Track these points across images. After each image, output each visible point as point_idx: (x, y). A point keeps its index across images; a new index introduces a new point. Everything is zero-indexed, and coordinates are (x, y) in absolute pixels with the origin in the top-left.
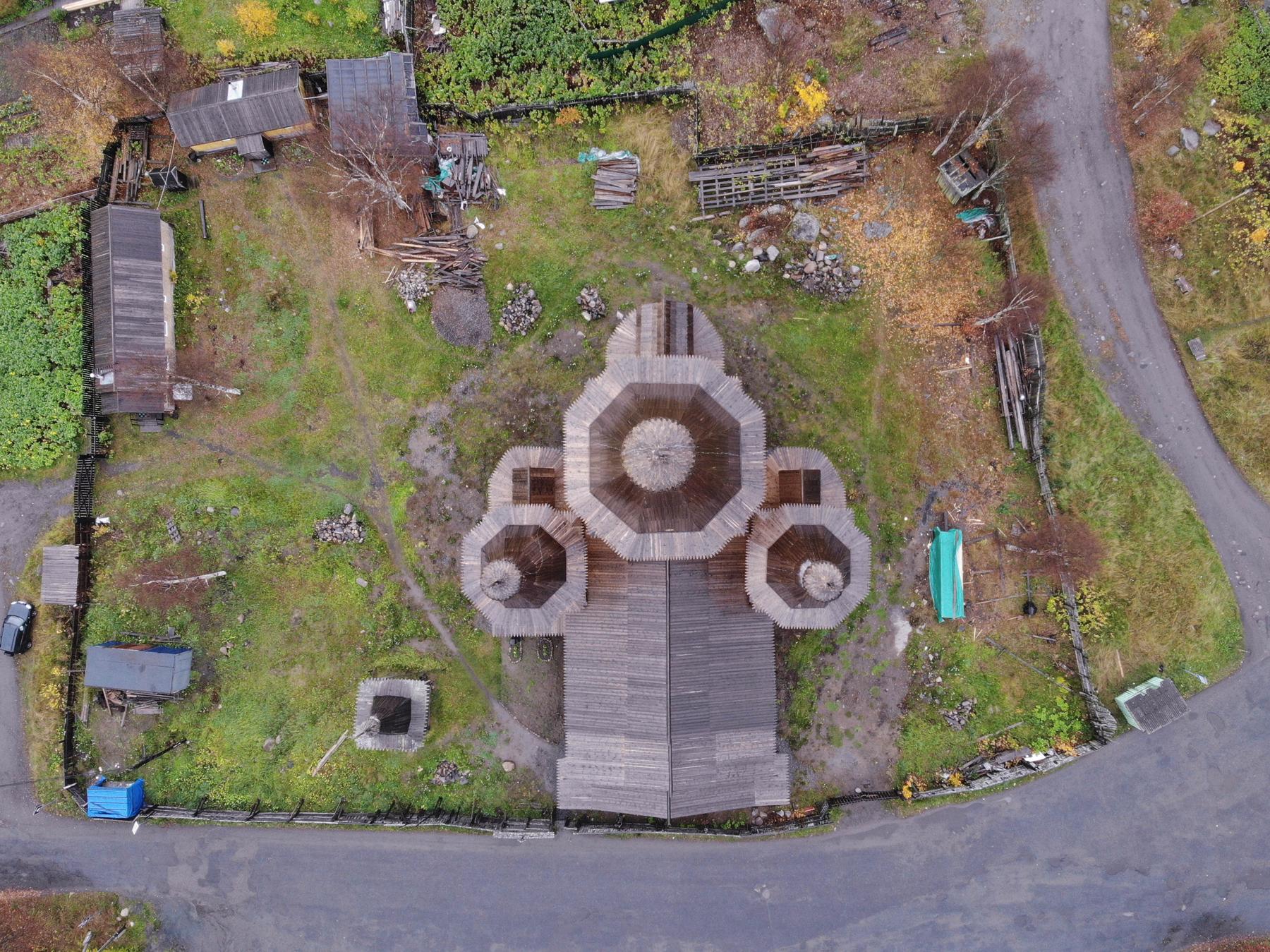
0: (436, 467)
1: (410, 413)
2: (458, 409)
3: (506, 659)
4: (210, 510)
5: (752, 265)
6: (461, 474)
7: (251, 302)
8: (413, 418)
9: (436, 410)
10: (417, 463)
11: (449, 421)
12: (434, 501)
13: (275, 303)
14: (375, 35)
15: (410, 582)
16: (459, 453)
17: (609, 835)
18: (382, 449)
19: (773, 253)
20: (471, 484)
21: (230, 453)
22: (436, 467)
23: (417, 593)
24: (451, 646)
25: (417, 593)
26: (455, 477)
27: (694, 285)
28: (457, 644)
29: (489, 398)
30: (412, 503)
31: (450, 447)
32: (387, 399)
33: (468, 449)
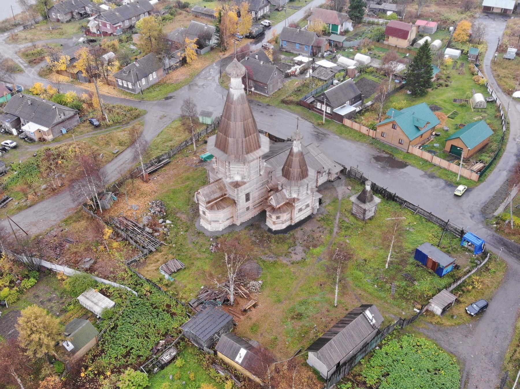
0: (299, 249)
1: (292, 266)
2: (277, 256)
3: (327, 204)
4: (376, 286)
5: (168, 222)
6: (295, 243)
7: (305, 322)
8: (292, 263)
9: (285, 261)
10: (303, 254)
11: (284, 255)
12: (308, 241)
13: (299, 316)
14: (64, 172)
15: (335, 233)
16: (290, 247)
17: (341, 108)
18: (309, 264)
19: (161, 221)
20: (294, 238)
21: (355, 295)
22: (299, 249)
23: (336, 230)
24: (338, 214)
25: (336, 230)
26: (297, 243)
27: (186, 231)
28: (337, 214)
29: (267, 251)
30: (315, 246)
31: (290, 250)
32: (294, 273)
33: (286, 246)
